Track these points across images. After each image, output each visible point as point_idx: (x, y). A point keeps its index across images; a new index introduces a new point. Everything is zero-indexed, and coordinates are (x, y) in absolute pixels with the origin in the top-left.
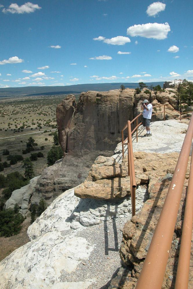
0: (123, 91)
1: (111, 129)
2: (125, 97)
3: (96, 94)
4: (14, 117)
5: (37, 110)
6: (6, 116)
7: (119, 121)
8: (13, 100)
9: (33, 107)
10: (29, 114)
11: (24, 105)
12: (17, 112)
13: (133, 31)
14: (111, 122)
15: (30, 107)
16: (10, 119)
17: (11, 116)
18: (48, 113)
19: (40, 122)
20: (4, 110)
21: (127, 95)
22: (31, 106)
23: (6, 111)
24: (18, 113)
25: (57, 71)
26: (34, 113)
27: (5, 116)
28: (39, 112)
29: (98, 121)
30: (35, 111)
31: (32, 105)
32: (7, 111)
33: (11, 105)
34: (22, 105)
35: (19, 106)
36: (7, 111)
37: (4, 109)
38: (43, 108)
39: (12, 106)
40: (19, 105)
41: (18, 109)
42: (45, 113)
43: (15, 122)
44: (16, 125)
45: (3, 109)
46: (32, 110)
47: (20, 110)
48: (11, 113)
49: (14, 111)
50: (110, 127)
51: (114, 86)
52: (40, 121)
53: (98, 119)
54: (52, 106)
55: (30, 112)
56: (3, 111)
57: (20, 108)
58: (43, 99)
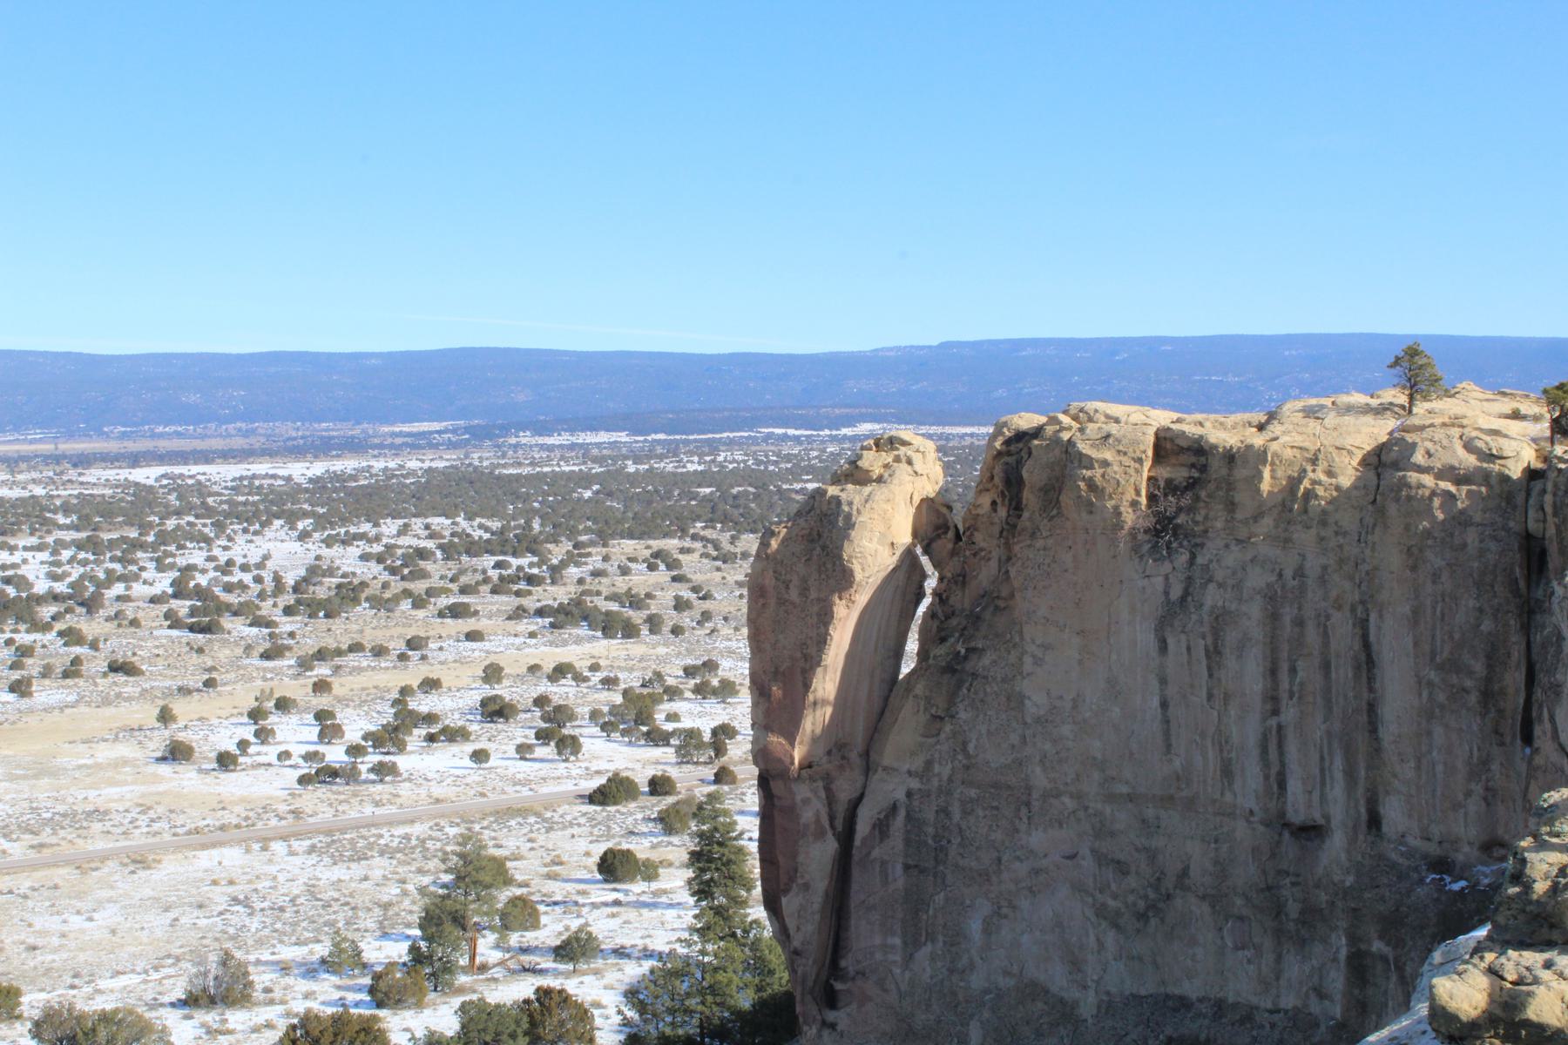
0: (1420, 408)
1: (1294, 786)
2: (1440, 475)
3: (1151, 432)
4: (308, 634)
5: (532, 580)
6: (238, 628)
7: (1372, 708)
8: (310, 474)
9: (500, 544)
10: (456, 612)
11: (417, 524)
12: (339, 586)
13: (987, 930)
14: (1289, 714)
15: (474, 548)
16: (266, 656)
17: (286, 625)
18: (644, 614)
19: (562, 692)
20: (223, 560)
21: (1461, 452)
22: (477, 534)
23: (237, 576)
24: (350, 593)
25: (617, 613)
26: (507, 602)
27: (227, 622)
28: (558, 595)
29: (1164, 705)
30: (522, 586)
31: (495, 525)
32: (247, 578)
33: (291, 519)
34: (389, 527)
35: (362, 536)
36: (247, 578)
37: (216, 552)
38: (595, 562)
39: (300, 525)
40: (366, 527)
41: (348, 559)
42: (614, 607)
43: (321, 686)
44: (321, 716)
45: (210, 559)
46: (494, 574)
47: (372, 571)
48: (288, 599)
49: (315, 572)
50: (1283, 764)
51: (1319, 365)
52: (568, 680)
53: (1163, 681)
54: (687, 543)
55: (464, 590)
56: (212, 574)
57: (377, 548)
58: (597, 469)
